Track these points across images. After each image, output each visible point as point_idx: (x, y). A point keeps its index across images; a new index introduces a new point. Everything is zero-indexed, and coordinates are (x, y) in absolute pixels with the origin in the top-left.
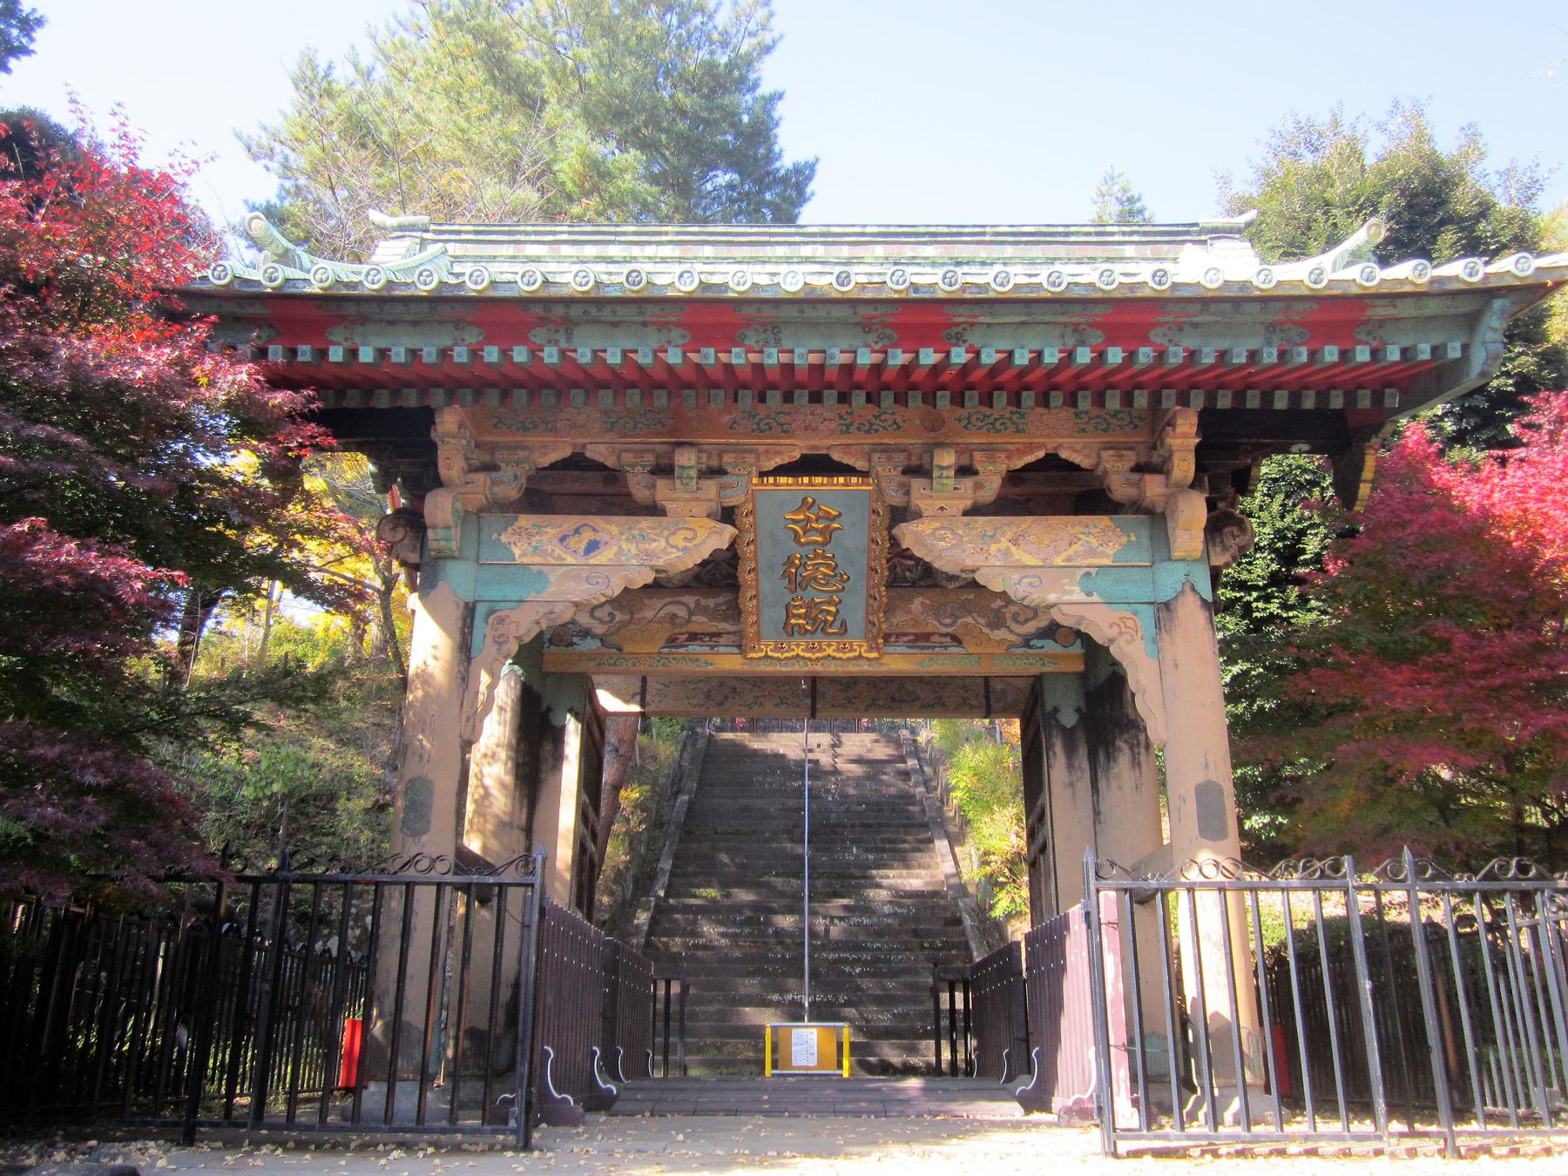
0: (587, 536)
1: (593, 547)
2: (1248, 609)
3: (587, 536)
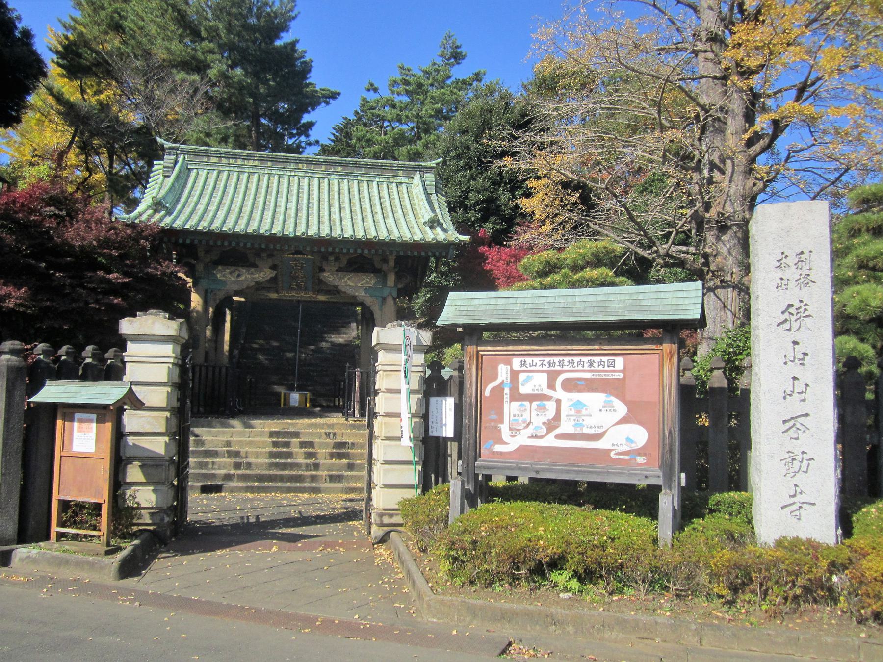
0: (237, 273)
1: (239, 276)
2: (449, 265)
3: (237, 273)
